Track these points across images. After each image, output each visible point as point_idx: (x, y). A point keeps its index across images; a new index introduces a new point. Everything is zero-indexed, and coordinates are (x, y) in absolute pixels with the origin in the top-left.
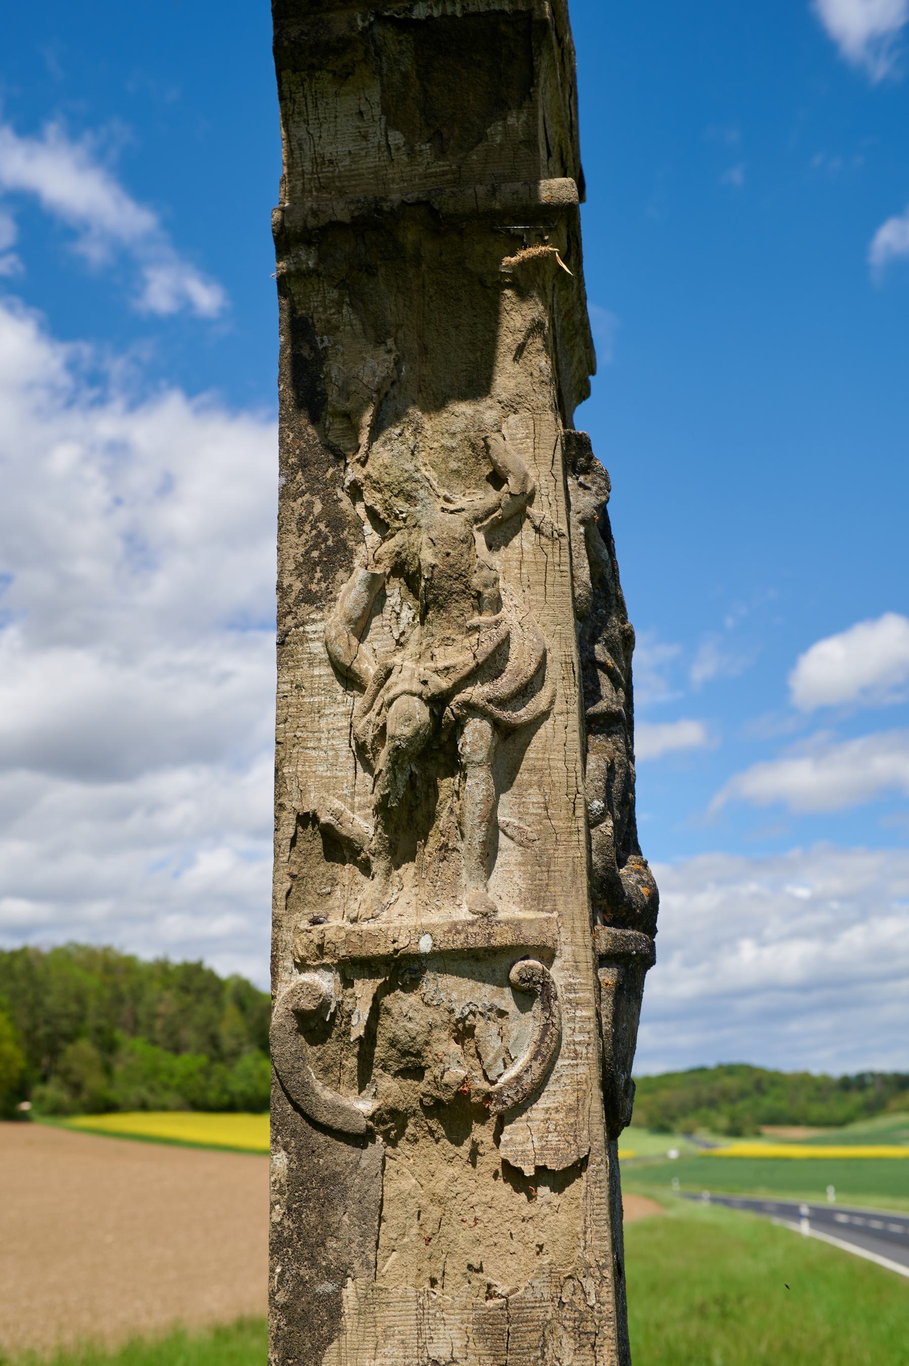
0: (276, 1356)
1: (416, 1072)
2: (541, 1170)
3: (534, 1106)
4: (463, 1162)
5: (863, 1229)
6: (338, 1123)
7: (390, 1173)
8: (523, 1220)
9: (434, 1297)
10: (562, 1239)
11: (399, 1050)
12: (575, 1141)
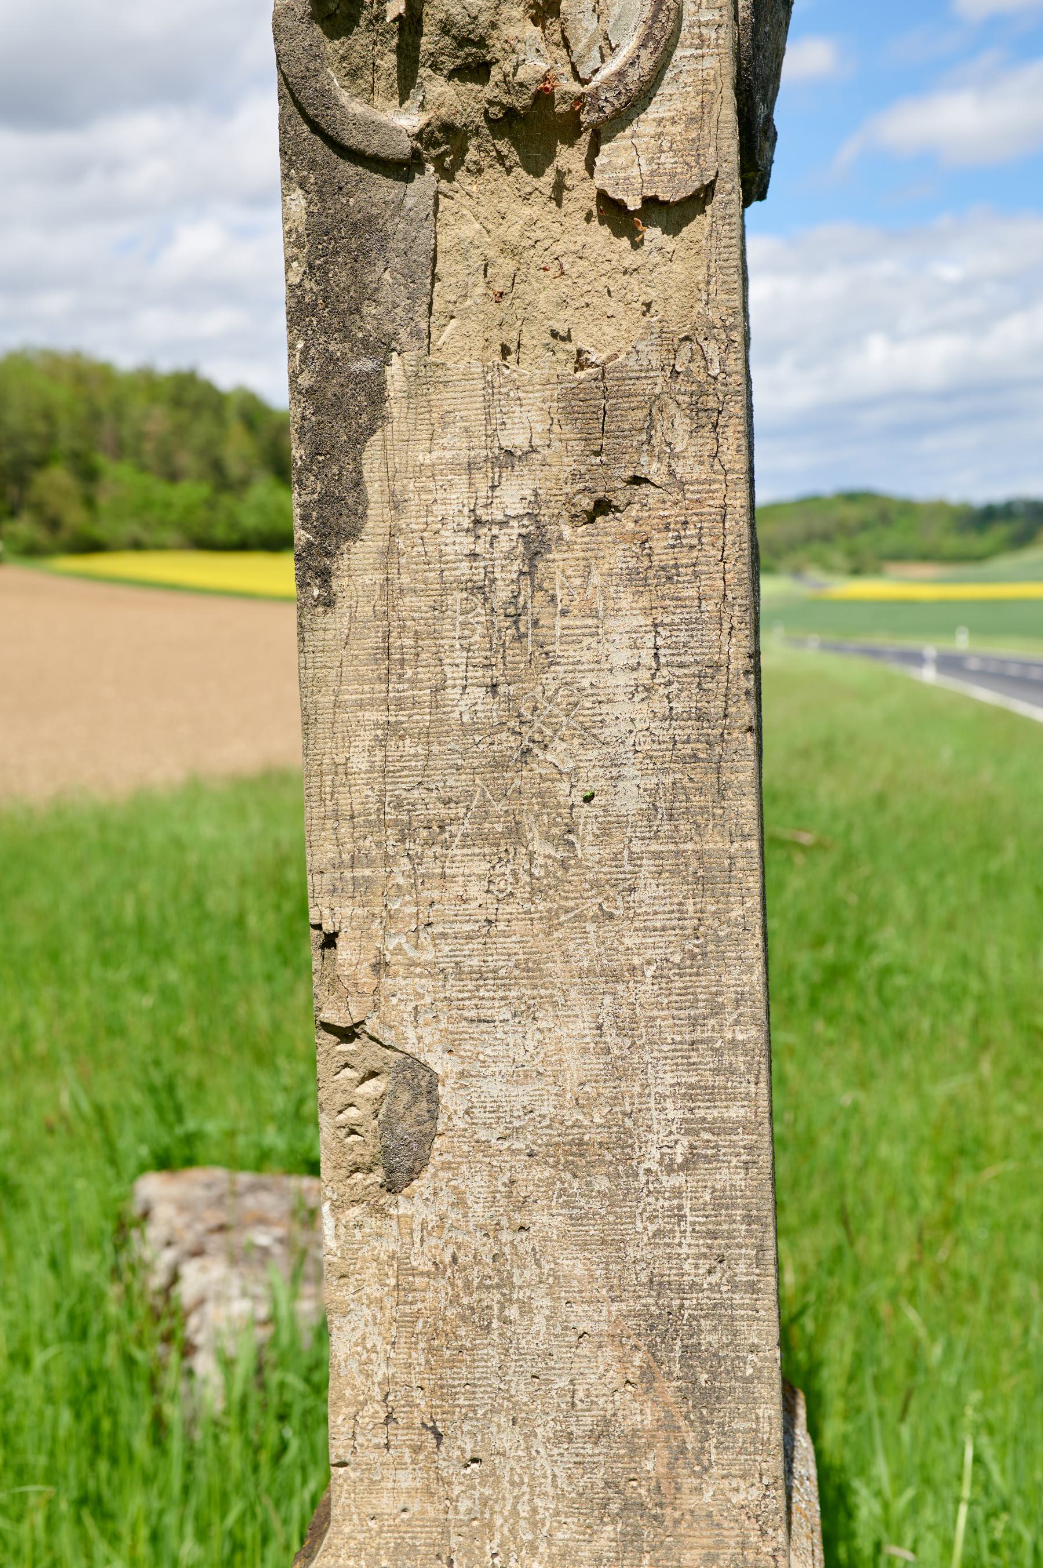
0: (303, 452)
1: (476, 71)
2: (651, 202)
3: (642, 116)
4: (544, 199)
5: (995, 674)
6: (373, 146)
7: (445, 216)
8: (625, 273)
9: (507, 372)
10: (677, 295)
11: (454, 38)
12: (698, 163)
